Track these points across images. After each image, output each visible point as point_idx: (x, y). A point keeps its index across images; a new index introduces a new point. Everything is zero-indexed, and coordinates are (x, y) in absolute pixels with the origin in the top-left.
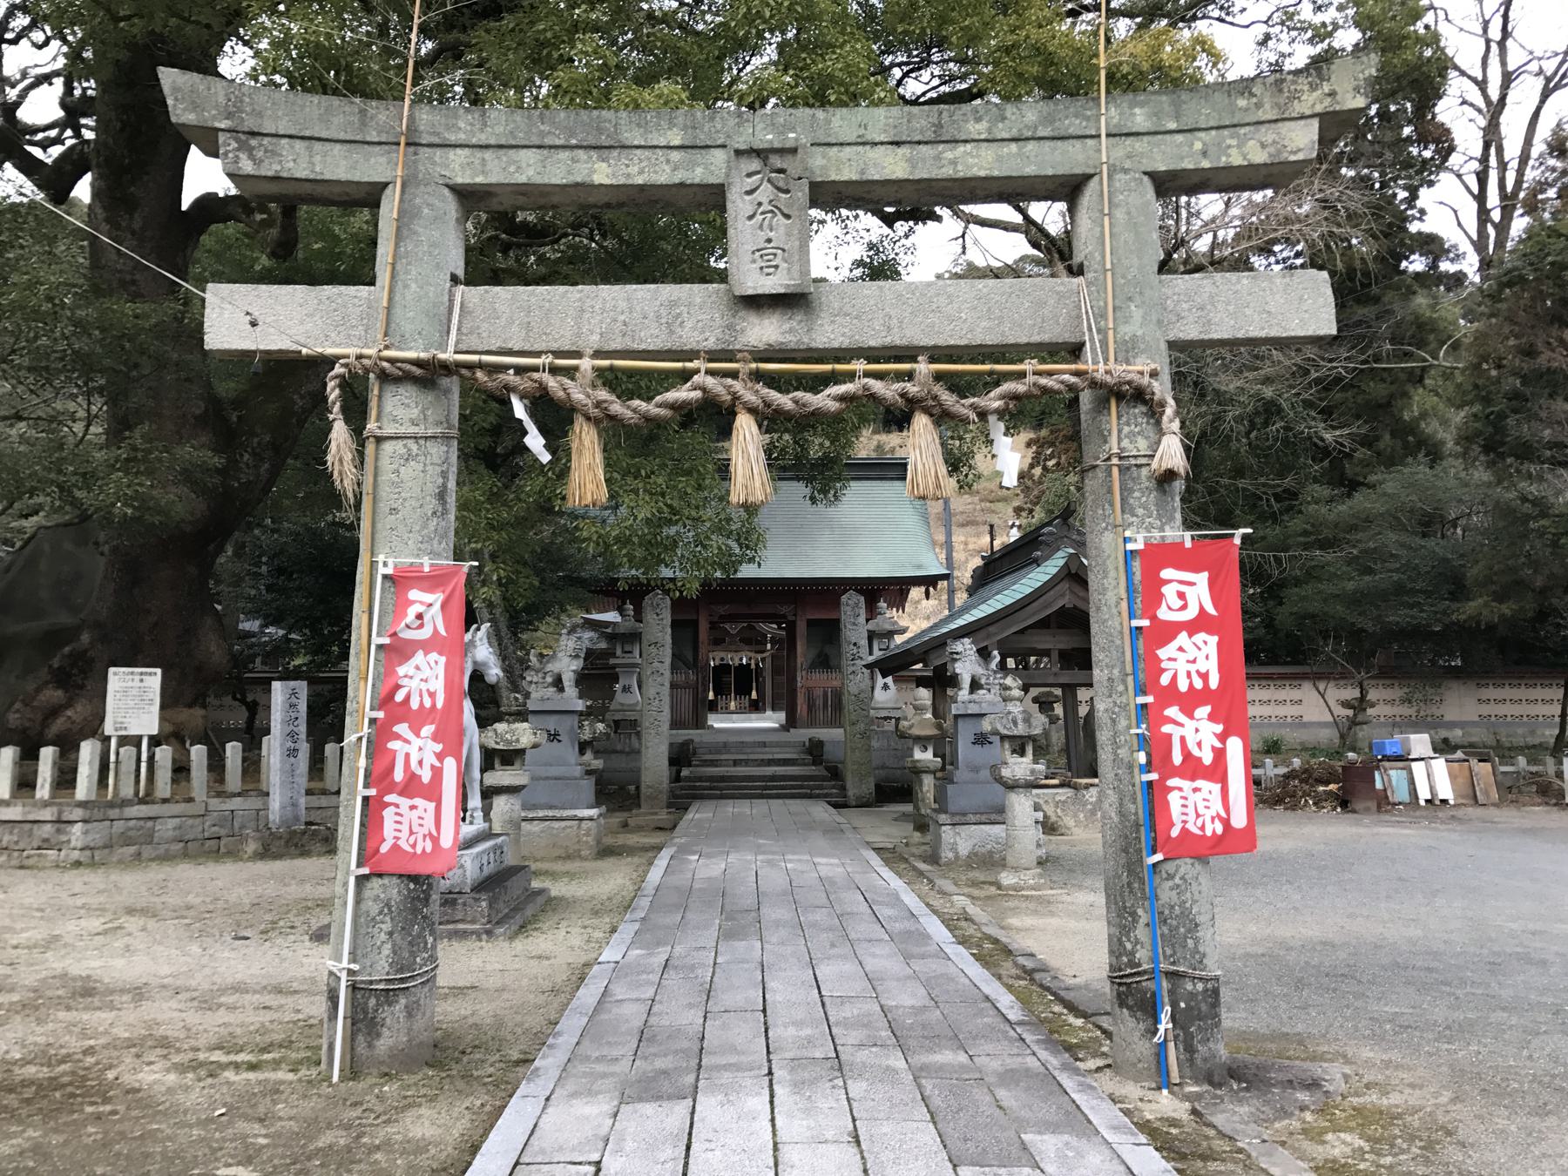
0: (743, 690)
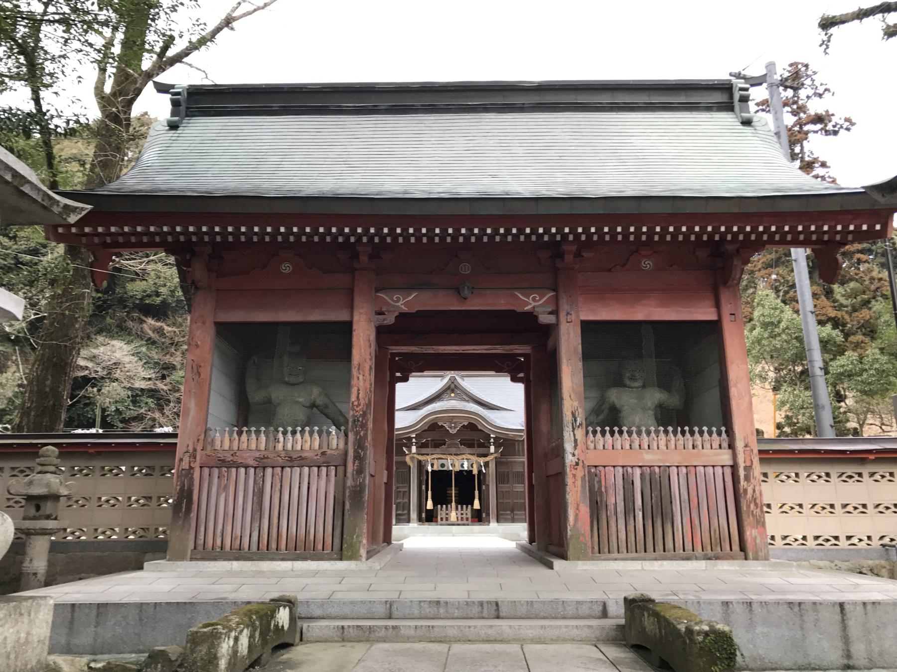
0: (465, 499)
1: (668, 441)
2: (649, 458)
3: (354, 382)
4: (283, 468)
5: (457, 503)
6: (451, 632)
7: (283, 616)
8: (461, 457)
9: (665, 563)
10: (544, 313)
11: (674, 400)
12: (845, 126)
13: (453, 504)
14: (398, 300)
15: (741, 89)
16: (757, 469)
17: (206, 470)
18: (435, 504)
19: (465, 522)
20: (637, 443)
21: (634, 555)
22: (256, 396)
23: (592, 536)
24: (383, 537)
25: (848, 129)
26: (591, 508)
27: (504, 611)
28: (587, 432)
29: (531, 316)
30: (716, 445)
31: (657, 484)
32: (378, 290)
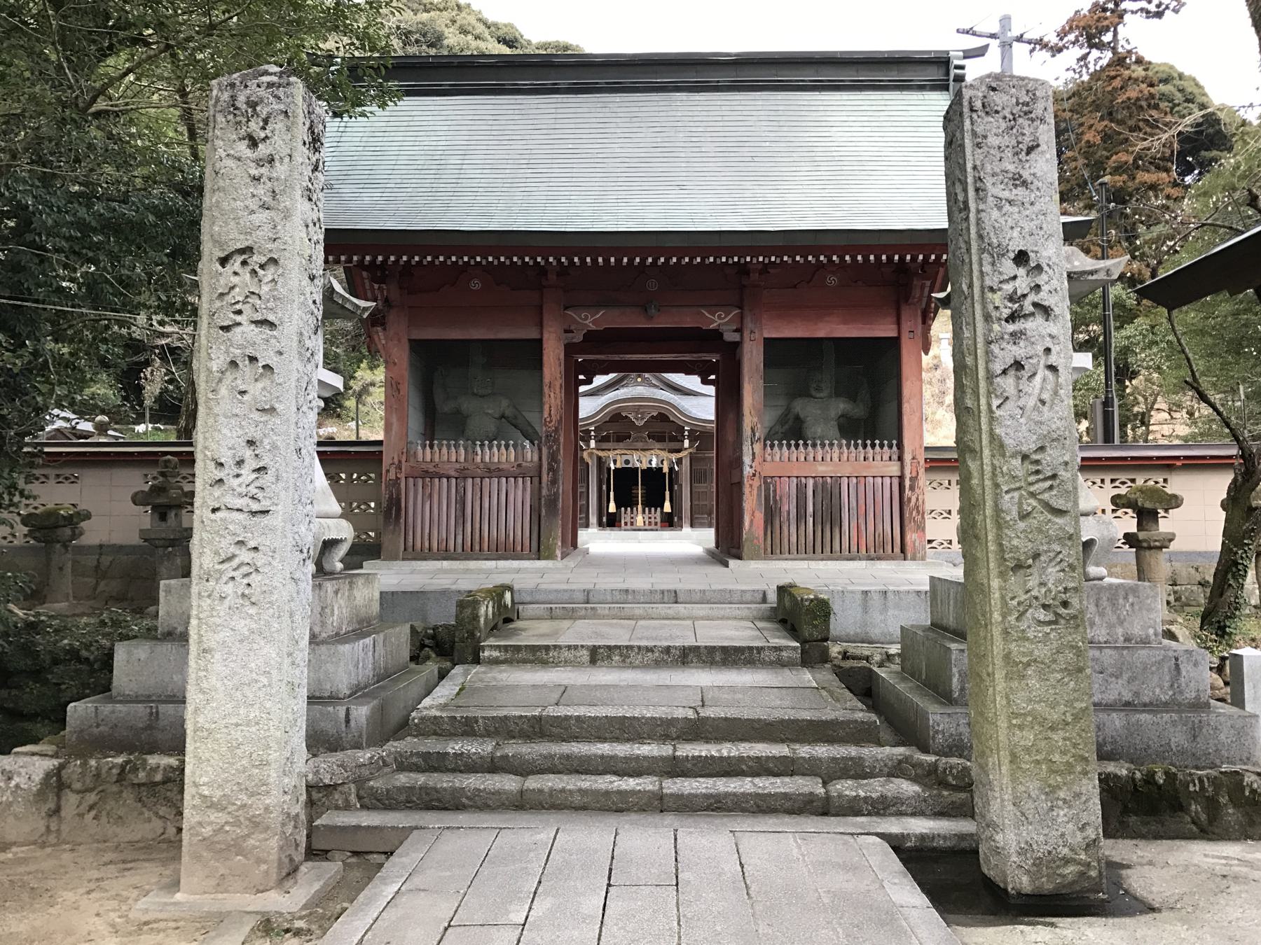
0: (654, 501)
1: (841, 453)
2: (822, 469)
3: (546, 399)
4: (482, 478)
5: (645, 505)
6: (637, 612)
7: (508, 595)
8: (648, 453)
9: (829, 562)
10: (728, 331)
11: (858, 411)
12: (1171, 7)
13: (640, 506)
14: (586, 318)
15: (957, 67)
16: (923, 479)
17: (411, 480)
18: (618, 507)
19: (653, 527)
20: (812, 455)
21: (804, 556)
22: (445, 407)
23: (765, 539)
24: (572, 543)
25: (1176, 11)
26: (765, 514)
27: (681, 597)
28: (765, 445)
29: (717, 334)
30: (886, 457)
31: (829, 494)
32: (566, 308)
